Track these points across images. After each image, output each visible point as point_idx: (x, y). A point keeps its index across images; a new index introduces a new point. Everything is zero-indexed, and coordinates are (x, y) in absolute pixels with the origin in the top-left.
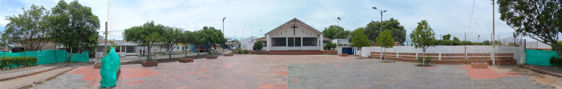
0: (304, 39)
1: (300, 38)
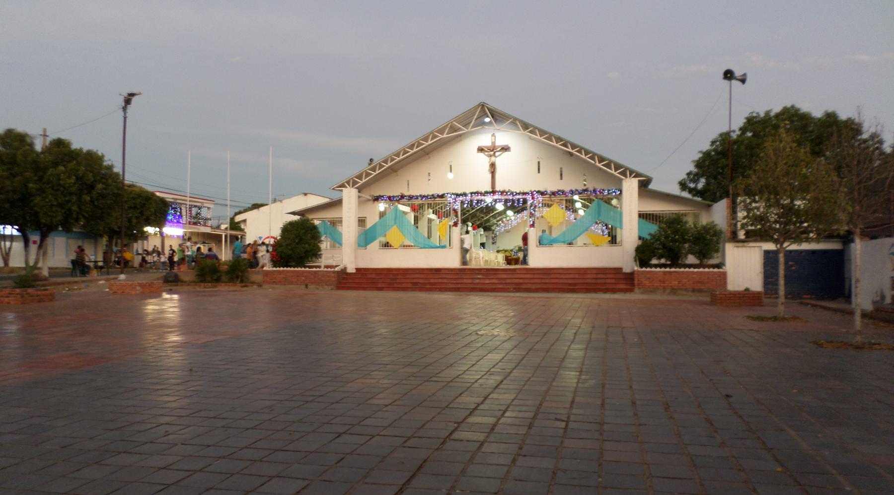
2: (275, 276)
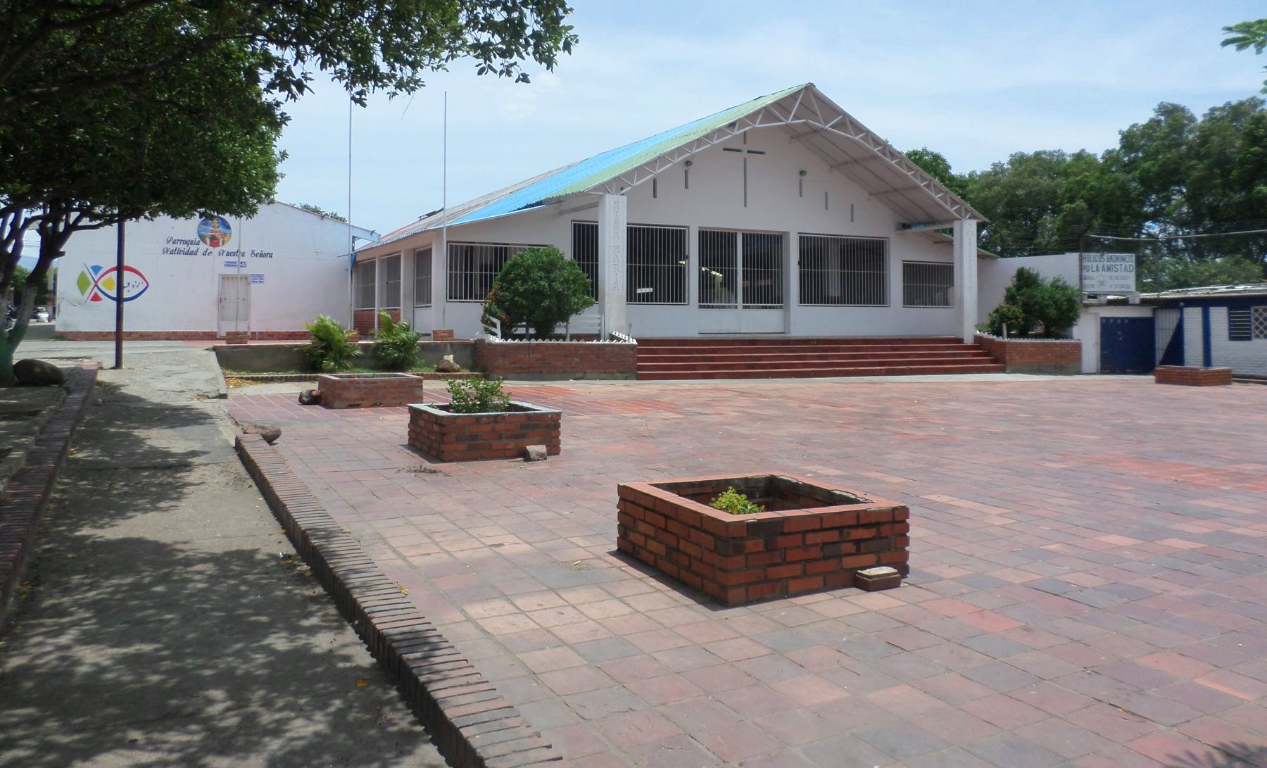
0: (813, 249)
1: (776, 240)
2: (521, 356)
